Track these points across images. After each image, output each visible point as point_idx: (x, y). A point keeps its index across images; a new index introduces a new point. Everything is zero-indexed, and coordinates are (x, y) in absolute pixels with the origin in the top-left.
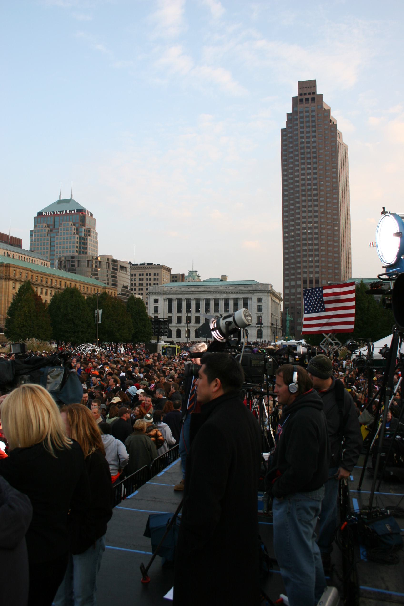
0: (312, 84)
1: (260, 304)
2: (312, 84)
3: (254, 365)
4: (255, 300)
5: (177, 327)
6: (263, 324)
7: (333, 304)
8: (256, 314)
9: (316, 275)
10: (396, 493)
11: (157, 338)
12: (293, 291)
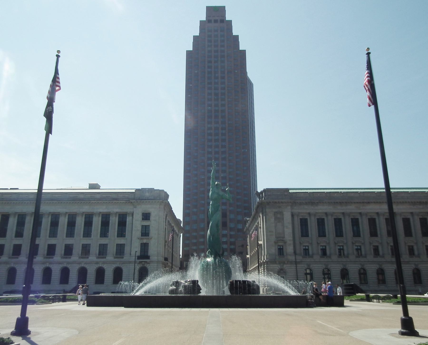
0: (221, 10)
1: (146, 223)
2: (221, 10)
4: (138, 217)
5: (79, 263)
6: (150, 258)
7: (181, 248)
8: (138, 241)
11: (134, 263)
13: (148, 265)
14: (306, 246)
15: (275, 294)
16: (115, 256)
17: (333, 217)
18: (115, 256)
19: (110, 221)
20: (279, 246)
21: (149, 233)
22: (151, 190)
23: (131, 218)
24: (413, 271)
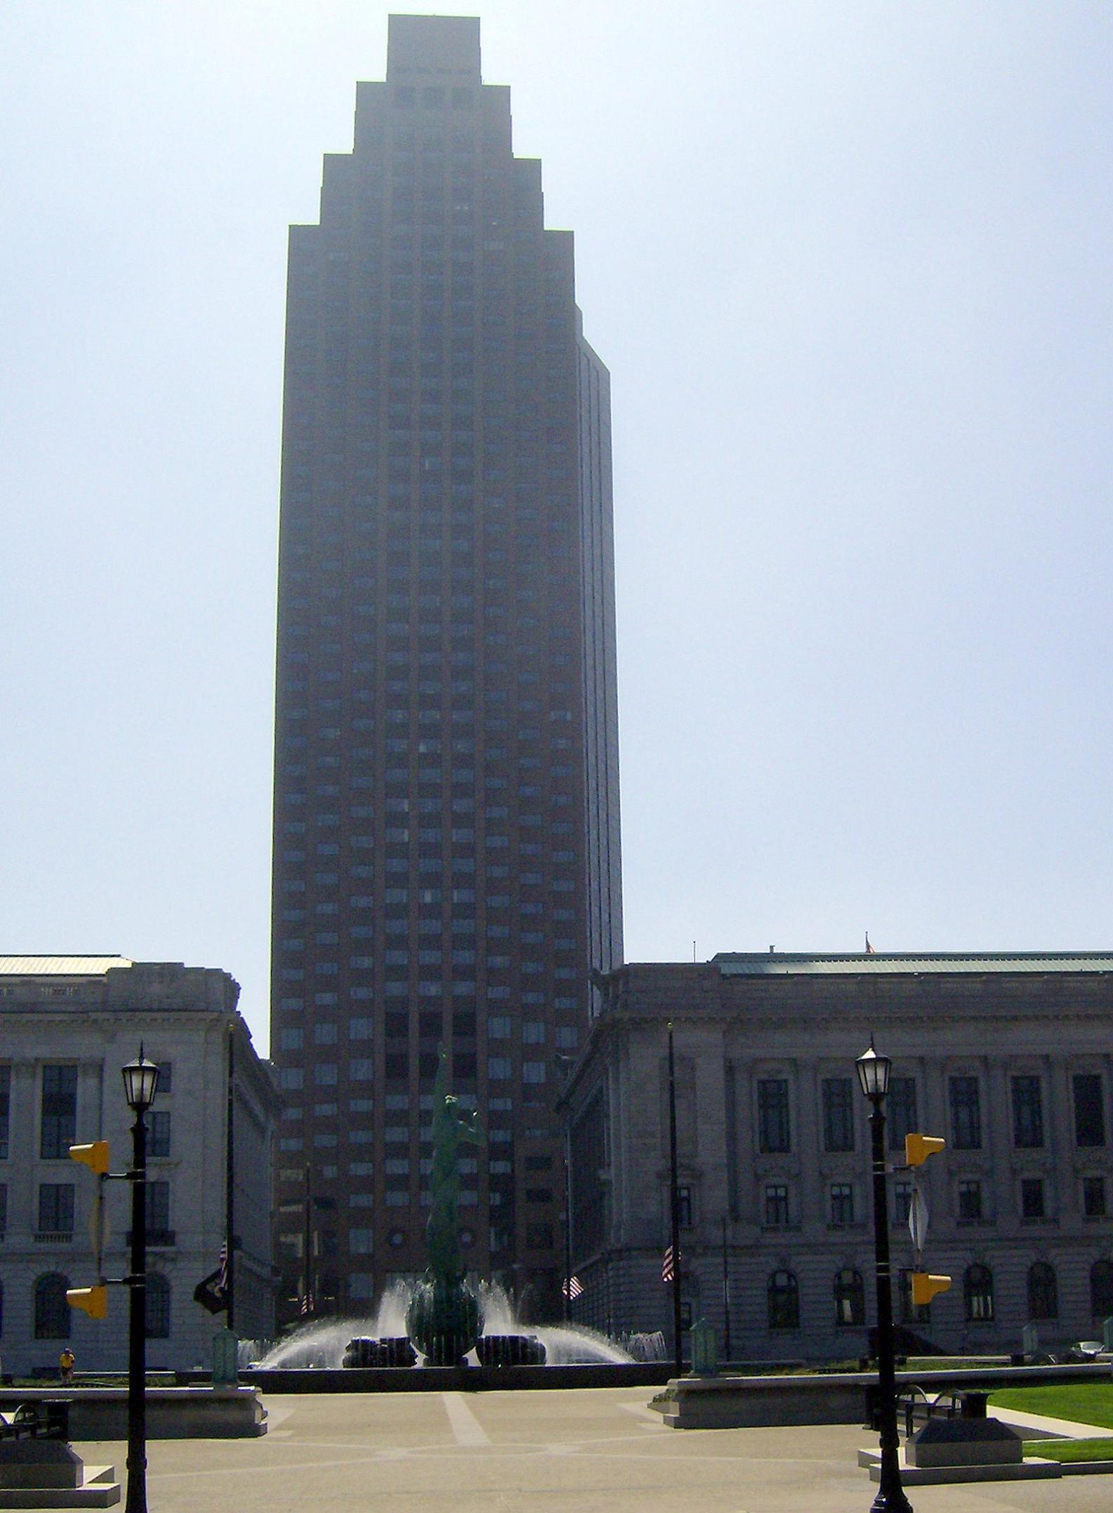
3: (856, 1360)
6: (178, 1238)
9: (462, 988)
10: (5, 1388)
12: (328, 1076)
13: (169, 1266)
14: (780, 1186)
15: (61, 1387)
16: (37, 1232)
17: (1071, 1073)
18: (37, 1232)
19: (12, 1096)
20: (771, 1187)
21: (168, 1141)
22: (171, 972)
23: (93, 1082)
24: (1094, 1270)
